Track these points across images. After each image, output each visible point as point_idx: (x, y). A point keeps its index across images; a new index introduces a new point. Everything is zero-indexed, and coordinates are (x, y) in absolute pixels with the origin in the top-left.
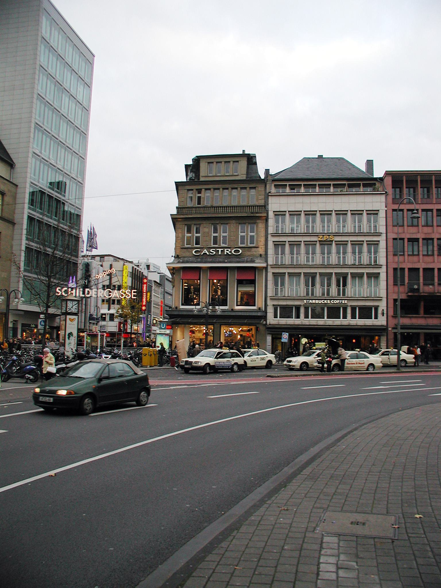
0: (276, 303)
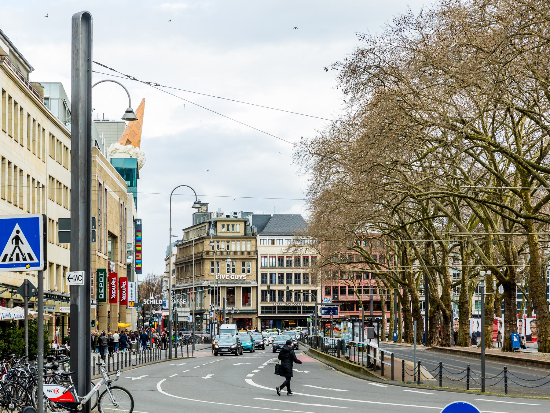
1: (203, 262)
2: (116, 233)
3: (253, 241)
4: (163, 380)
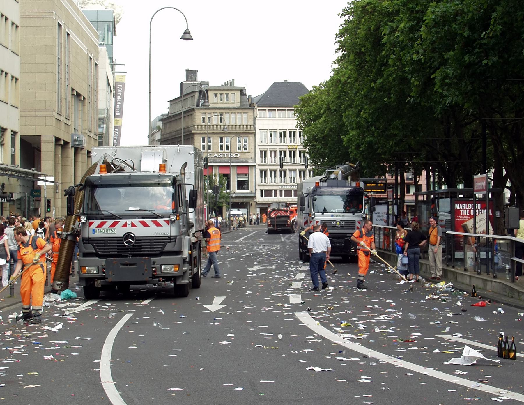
0: (262, 188)
1: (193, 138)
2: (84, 93)
3: (251, 113)
4: (29, 374)
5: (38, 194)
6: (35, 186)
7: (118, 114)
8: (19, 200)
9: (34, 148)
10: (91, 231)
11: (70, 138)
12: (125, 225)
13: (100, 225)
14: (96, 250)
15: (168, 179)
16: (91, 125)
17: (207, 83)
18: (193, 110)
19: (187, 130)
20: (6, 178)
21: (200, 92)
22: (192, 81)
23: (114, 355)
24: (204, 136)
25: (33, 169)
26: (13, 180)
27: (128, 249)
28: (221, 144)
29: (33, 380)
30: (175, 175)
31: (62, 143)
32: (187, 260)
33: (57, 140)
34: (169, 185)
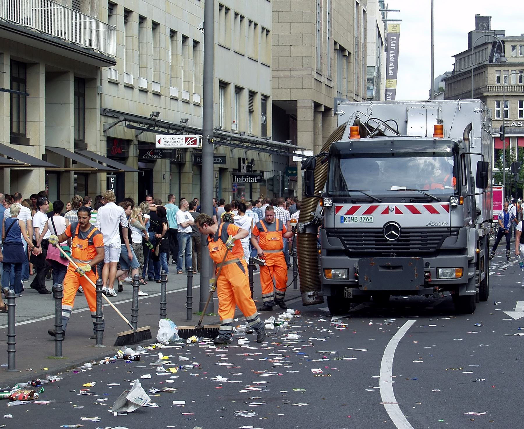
2: (349, 47)
4: (295, 390)
5: (293, 172)
6: (290, 163)
7: (391, 74)
8: (271, 180)
9: (288, 115)
10: (338, 220)
11: (333, 102)
12: (386, 212)
13: (351, 211)
14: (345, 247)
15: (446, 146)
16: (358, 86)
17: (503, 32)
18: (485, 66)
19: (477, 92)
20: (255, 152)
21: (494, 44)
22: (483, 30)
23: (395, 371)
24: (498, 99)
25: (288, 141)
26: (264, 156)
27: (390, 245)
28: (521, 109)
29: (300, 397)
30: (456, 141)
31: (323, 109)
32: (474, 261)
33: (317, 105)
34: (447, 155)
